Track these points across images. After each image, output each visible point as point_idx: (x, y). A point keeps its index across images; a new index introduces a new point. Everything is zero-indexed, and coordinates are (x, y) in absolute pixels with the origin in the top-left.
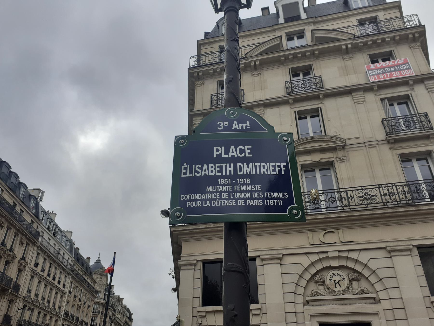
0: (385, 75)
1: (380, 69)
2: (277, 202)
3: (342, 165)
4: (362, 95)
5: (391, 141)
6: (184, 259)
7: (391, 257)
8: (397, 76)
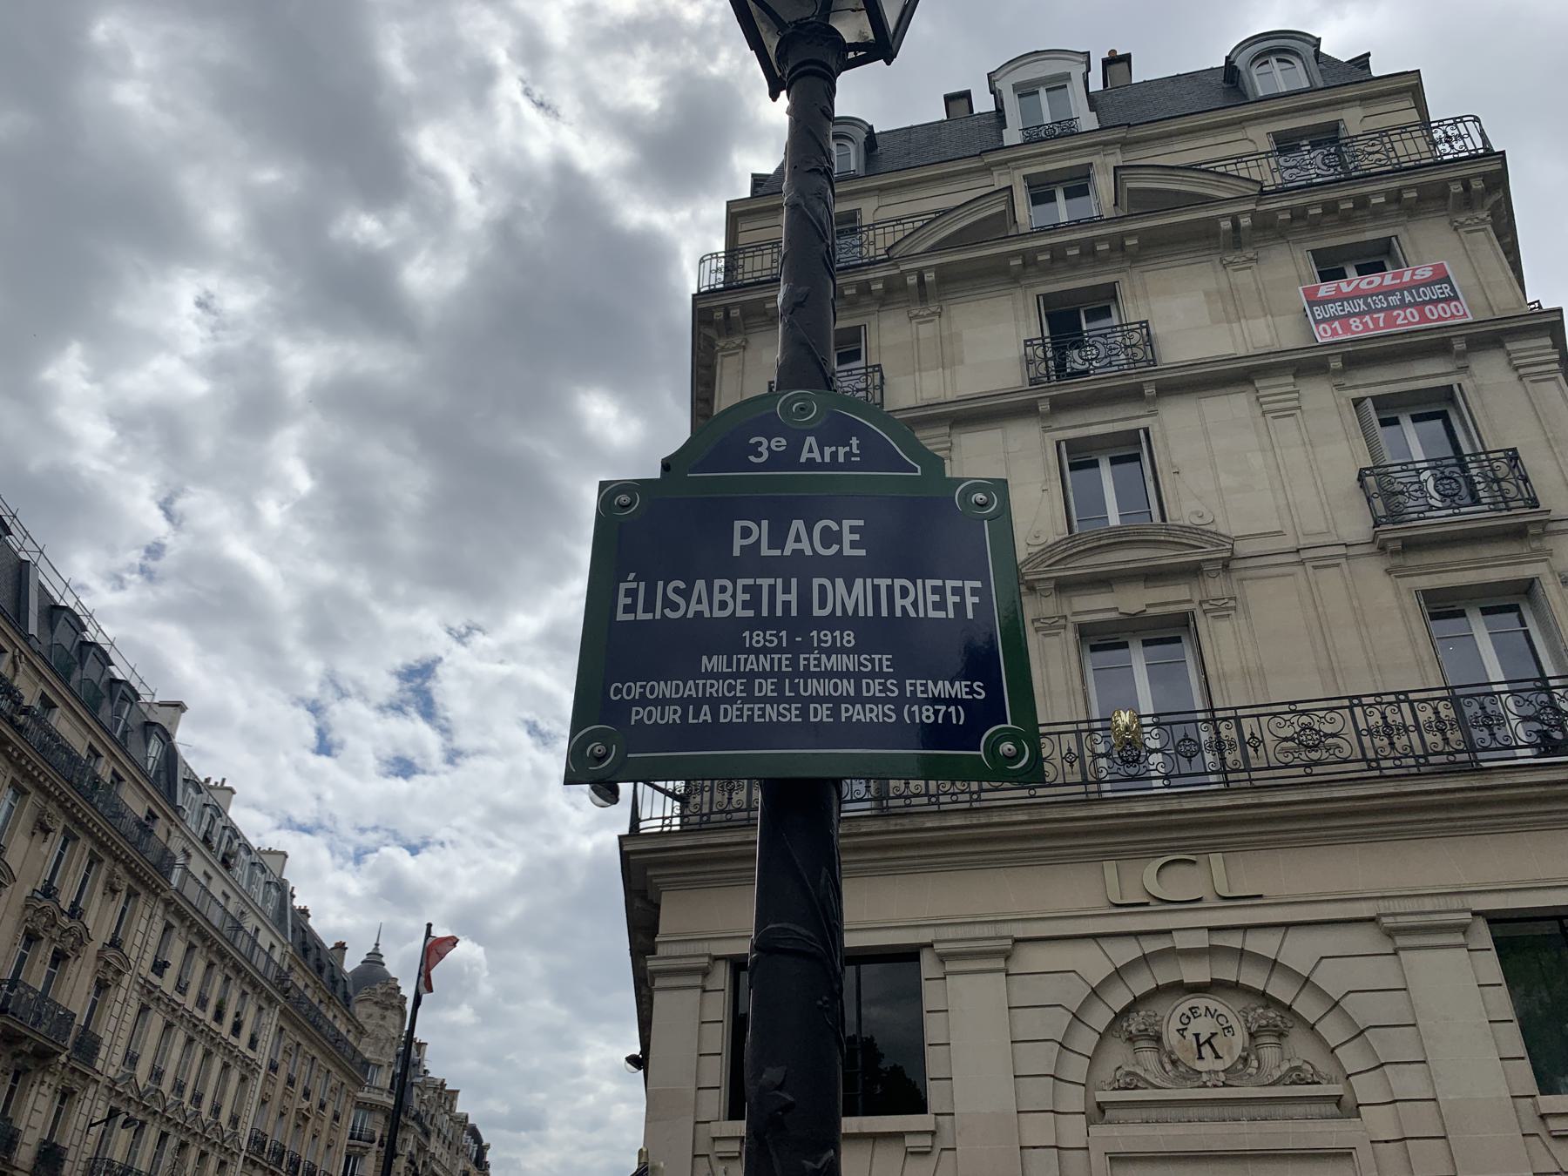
0: (1367, 318)
1: (1353, 298)
2: (947, 715)
3: (1223, 626)
4: (1291, 388)
5: (1391, 546)
6: (666, 952)
7: (1395, 953)
8: (1410, 323)
